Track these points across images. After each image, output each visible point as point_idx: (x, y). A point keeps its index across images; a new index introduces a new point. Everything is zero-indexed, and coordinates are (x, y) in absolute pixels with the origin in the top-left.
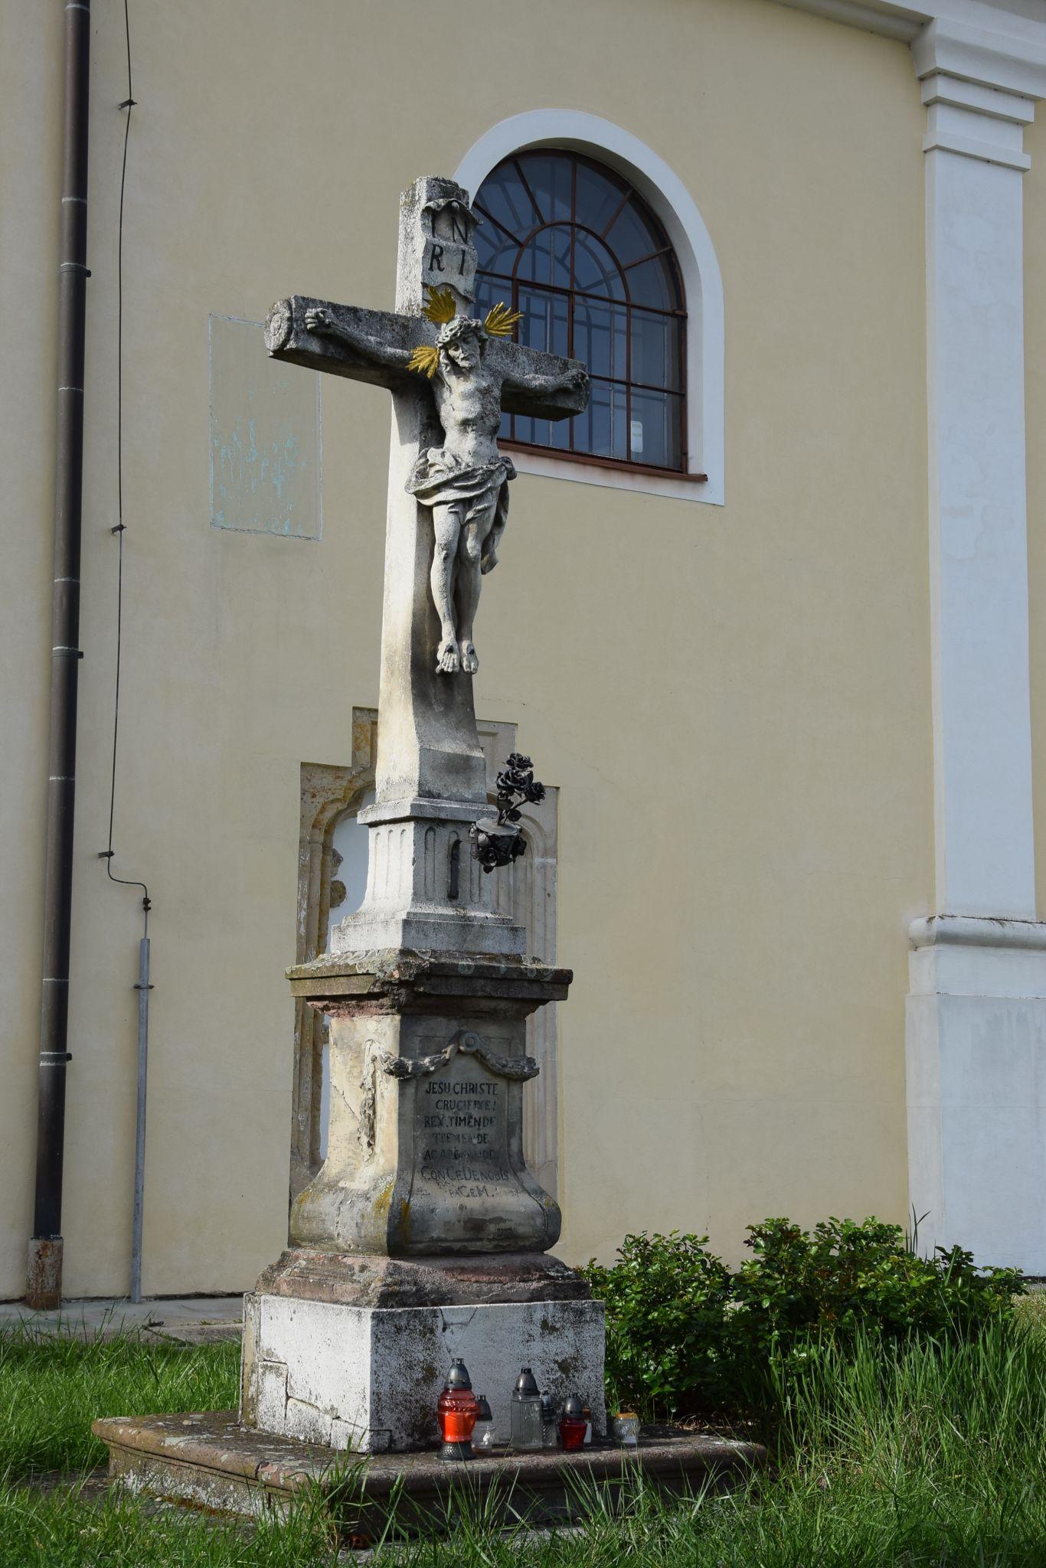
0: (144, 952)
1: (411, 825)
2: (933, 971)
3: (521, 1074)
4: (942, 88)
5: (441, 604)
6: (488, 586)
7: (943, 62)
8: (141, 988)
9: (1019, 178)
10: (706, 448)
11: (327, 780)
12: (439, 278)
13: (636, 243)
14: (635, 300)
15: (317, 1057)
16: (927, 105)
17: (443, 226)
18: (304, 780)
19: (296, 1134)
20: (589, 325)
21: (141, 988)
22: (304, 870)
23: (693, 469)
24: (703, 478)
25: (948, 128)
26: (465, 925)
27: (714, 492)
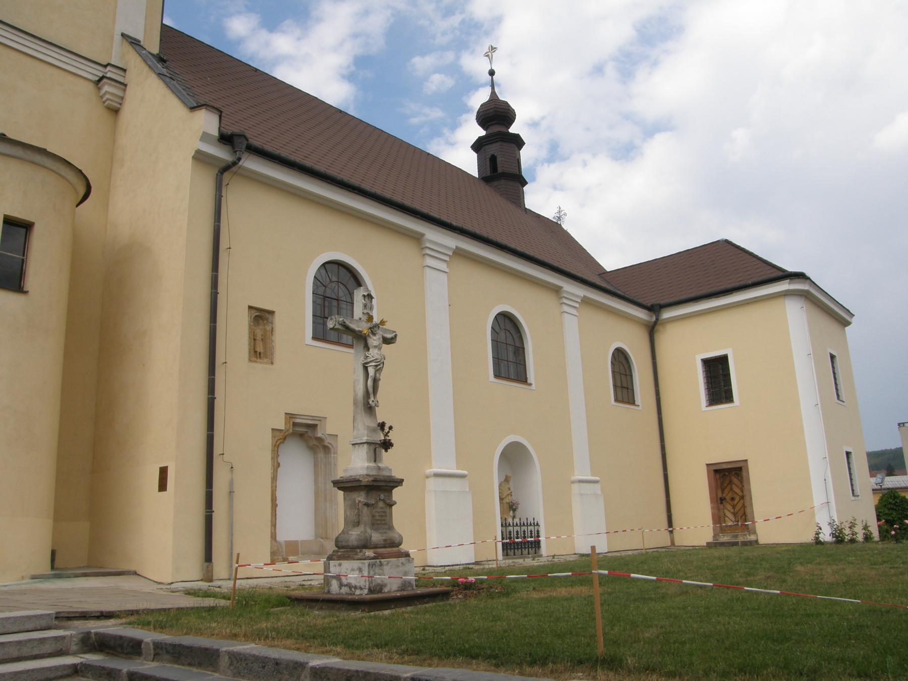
0: (231, 483)
1: (365, 446)
4: (428, 252)
6: (381, 384)
7: (428, 245)
8: (231, 492)
9: (445, 276)
11: (277, 434)
12: (365, 311)
21: (231, 492)
25: (429, 261)
26: (379, 468)
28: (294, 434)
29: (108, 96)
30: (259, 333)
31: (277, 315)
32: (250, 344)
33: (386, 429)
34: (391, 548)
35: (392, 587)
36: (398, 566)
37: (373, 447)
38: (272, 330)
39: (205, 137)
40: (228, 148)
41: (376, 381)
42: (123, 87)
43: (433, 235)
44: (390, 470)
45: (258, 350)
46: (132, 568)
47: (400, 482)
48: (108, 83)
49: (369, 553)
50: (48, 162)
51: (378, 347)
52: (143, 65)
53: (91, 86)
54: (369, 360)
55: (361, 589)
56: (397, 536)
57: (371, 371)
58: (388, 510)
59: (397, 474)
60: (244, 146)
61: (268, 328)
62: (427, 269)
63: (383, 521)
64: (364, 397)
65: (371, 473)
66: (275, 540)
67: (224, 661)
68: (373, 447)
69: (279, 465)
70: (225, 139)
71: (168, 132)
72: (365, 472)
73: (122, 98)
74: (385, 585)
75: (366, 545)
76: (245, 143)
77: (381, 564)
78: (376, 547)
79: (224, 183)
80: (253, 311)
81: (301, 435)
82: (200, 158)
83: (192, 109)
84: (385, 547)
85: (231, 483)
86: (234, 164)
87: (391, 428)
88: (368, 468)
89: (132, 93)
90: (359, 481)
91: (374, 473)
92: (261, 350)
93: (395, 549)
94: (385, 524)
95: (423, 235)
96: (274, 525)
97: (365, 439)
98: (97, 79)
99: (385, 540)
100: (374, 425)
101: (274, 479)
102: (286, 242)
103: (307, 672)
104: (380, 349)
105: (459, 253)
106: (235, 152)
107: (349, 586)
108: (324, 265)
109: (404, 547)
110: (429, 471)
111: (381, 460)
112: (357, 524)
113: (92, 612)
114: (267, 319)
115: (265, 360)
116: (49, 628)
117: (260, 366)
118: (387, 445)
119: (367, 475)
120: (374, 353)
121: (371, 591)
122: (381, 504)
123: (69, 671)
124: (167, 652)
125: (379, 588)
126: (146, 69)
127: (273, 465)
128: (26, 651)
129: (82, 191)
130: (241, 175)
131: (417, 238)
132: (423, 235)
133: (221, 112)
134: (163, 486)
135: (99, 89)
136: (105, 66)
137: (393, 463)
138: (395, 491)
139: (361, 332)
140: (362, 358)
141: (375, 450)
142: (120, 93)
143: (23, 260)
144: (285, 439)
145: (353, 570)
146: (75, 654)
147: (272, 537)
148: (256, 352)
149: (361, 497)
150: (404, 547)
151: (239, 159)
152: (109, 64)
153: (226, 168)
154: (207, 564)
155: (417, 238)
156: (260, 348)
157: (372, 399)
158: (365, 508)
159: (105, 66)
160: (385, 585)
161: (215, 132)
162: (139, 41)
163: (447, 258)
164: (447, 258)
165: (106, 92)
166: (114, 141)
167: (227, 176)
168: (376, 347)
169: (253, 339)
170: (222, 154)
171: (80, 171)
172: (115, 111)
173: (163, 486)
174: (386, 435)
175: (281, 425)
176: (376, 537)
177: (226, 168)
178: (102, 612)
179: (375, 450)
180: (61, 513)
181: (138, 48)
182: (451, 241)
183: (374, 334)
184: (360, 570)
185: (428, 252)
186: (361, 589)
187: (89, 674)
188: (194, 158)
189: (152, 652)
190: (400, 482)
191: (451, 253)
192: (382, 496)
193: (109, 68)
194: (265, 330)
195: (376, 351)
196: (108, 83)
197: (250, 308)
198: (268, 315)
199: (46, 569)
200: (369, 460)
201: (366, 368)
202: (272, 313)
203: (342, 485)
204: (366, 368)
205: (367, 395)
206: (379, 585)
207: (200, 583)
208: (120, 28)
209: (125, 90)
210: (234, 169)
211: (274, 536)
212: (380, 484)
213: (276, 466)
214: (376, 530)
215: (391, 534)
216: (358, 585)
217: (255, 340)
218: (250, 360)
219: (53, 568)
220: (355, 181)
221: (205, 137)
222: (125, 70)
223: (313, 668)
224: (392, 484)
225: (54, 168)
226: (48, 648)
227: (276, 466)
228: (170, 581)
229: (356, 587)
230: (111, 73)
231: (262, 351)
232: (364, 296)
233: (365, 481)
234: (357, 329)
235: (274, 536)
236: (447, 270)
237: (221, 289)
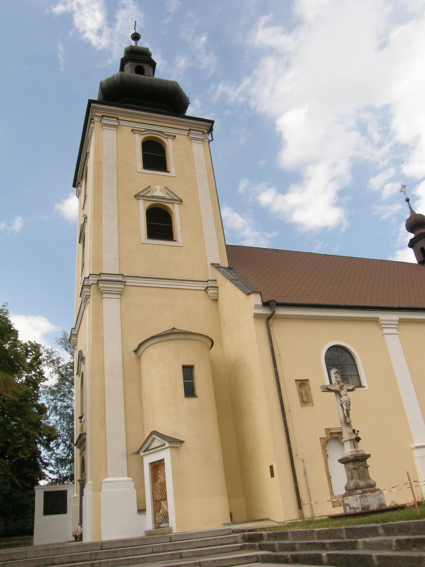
0: (304, 469)
1: (349, 441)
2: (416, 453)
3: (367, 468)
4: (383, 326)
5: (346, 415)
6: (350, 412)
7: (382, 323)
8: (305, 473)
9: (397, 336)
10: (364, 382)
11: (323, 440)
12: (337, 380)
13: (348, 356)
14: (349, 364)
15: (330, 480)
16: (382, 328)
17: (336, 374)
18: (320, 440)
19: (330, 491)
20: (343, 368)
21: (305, 473)
22: (323, 453)
23: (363, 385)
24: (364, 387)
25: (386, 331)
26: (357, 451)
27: (367, 388)
28: (332, 438)
29: (211, 295)
30: (303, 391)
31: (310, 380)
32: (300, 398)
33: (356, 433)
34: (371, 488)
35: (374, 506)
36: (375, 496)
37: (352, 441)
38: (309, 389)
39: (256, 307)
40: (268, 308)
41: (348, 411)
42: (217, 289)
43: (383, 316)
44: (363, 451)
45: (304, 400)
46: (266, 517)
47: (369, 456)
48: (210, 289)
49: (359, 491)
50: (194, 337)
51: (346, 395)
52: (223, 276)
53: (203, 292)
54: (342, 402)
55: (358, 509)
56: (372, 482)
57: (345, 407)
58: (366, 470)
59: (367, 453)
60: (275, 305)
61: (307, 388)
62: (386, 335)
63: (364, 475)
64: (344, 419)
65: (353, 454)
66: (333, 495)
67: (290, 535)
68: (352, 441)
69: (327, 456)
70: (266, 304)
71: (241, 307)
72: (350, 454)
73: (218, 294)
74: (370, 506)
75: (357, 488)
76: (275, 303)
77: (366, 496)
78: (362, 488)
79: (270, 325)
80: (298, 382)
81: (336, 438)
82: (256, 316)
83: (248, 294)
84: (367, 488)
85: (304, 469)
86: (272, 315)
87: (358, 431)
88: (351, 451)
89: (221, 290)
90: (348, 458)
91: (355, 453)
92: (306, 400)
93: (372, 488)
94: (366, 477)
95: (378, 318)
96: (331, 487)
97: (348, 438)
98: (205, 288)
99: (366, 485)
100: (351, 431)
101: (326, 463)
102: (305, 344)
103: (315, 533)
104: (347, 395)
105: (401, 321)
106: (272, 309)
107: (353, 508)
108: (329, 349)
109: (377, 487)
110: (413, 446)
111: (358, 447)
112: (352, 478)
113: (246, 530)
114: (306, 384)
115: (309, 404)
116: (230, 534)
117: (307, 408)
118: (358, 439)
119: (352, 455)
120: (344, 398)
121: (362, 509)
122: (361, 468)
123: (239, 548)
124: (272, 536)
125: (368, 507)
126: (225, 278)
127: (324, 456)
128: (224, 542)
129: (210, 344)
130: (278, 318)
131: (376, 321)
132: (378, 318)
133: (261, 293)
134: (272, 475)
135: (207, 292)
136: (207, 281)
137: (364, 447)
138: (367, 460)
139: (336, 390)
140: (339, 401)
141: (354, 442)
142: (215, 292)
143: (193, 382)
144: (327, 442)
145: (354, 500)
146: (241, 543)
147: (331, 494)
148: (303, 401)
149: (351, 466)
150: (377, 487)
151: (274, 312)
152: (209, 280)
153: (269, 318)
154: (300, 510)
155: (376, 321)
156: (305, 399)
157: (348, 419)
158: (354, 470)
159: (207, 281)
160: (370, 506)
161: (260, 303)
162: (219, 264)
163: (396, 326)
164: (396, 326)
165: (210, 294)
166: (218, 314)
167: (270, 321)
168: (344, 395)
169: (301, 395)
170: (266, 311)
171: (207, 336)
172: (216, 300)
173: (272, 475)
174: (357, 435)
175: (324, 436)
176: (362, 483)
177: (269, 318)
178: (250, 529)
179: (354, 442)
180: (231, 495)
181: (219, 268)
182: (395, 316)
183: (342, 389)
184: (356, 500)
185: (383, 326)
186: (358, 509)
187: (246, 548)
188: (254, 317)
189: (267, 537)
190: (369, 456)
191: (397, 323)
192: (361, 464)
193: (209, 282)
194: (306, 390)
195: (345, 397)
196: (210, 289)
197: (296, 380)
198: (305, 382)
199: (229, 521)
200: (352, 448)
201: (342, 406)
202: (307, 380)
203: (342, 461)
204: (342, 406)
205: (345, 418)
206: (366, 506)
207: (299, 520)
208: (209, 262)
209: (218, 290)
210: (274, 316)
211: (332, 493)
212: (358, 458)
213: (326, 456)
214: (361, 480)
215: (369, 481)
216: (357, 507)
217: (302, 395)
218: (302, 406)
219: (232, 521)
220: (334, 303)
221: (256, 307)
222: (216, 281)
223: (317, 531)
224: (365, 457)
225: (197, 339)
226: (231, 541)
227: (326, 456)
228: (284, 521)
229: (356, 508)
230: (210, 284)
231: (307, 400)
232: (335, 373)
233: (351, 458)
234: (334, 389)
235: (332, 493)
236: (397, 333)
237: (280, 375)
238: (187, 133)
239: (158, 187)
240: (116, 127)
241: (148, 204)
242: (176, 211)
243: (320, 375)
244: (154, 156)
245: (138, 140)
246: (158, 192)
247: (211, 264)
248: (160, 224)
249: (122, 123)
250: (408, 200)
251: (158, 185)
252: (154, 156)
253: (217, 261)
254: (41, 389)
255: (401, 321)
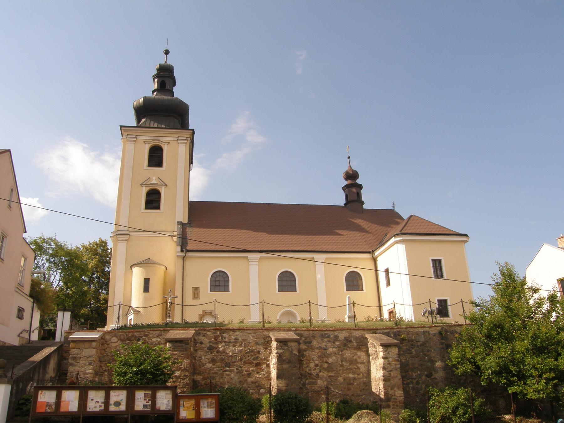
10: (297, 290)
30: (196, 293)
39: (178, 252)
131: (247, 258)
221: (178, 252)
238: (176, 139)
239: (154, 178)
240: (135, 141)
241: (148, 189)
242: (163, 191)
243: (206, 285)
244: (156, 157)
245: (147, 148)
246: (154, 181)
247: (178, 222)
248: (153, 200)
249: (138, 137)
250: (349, 158)
251: (154, 176)
252: (156, 157)
253: (181, 220)
254: (413, 338)
255: (261, 258)
